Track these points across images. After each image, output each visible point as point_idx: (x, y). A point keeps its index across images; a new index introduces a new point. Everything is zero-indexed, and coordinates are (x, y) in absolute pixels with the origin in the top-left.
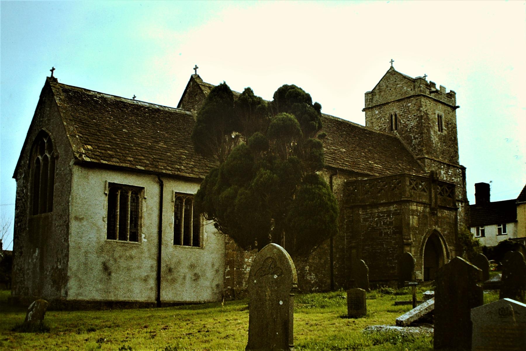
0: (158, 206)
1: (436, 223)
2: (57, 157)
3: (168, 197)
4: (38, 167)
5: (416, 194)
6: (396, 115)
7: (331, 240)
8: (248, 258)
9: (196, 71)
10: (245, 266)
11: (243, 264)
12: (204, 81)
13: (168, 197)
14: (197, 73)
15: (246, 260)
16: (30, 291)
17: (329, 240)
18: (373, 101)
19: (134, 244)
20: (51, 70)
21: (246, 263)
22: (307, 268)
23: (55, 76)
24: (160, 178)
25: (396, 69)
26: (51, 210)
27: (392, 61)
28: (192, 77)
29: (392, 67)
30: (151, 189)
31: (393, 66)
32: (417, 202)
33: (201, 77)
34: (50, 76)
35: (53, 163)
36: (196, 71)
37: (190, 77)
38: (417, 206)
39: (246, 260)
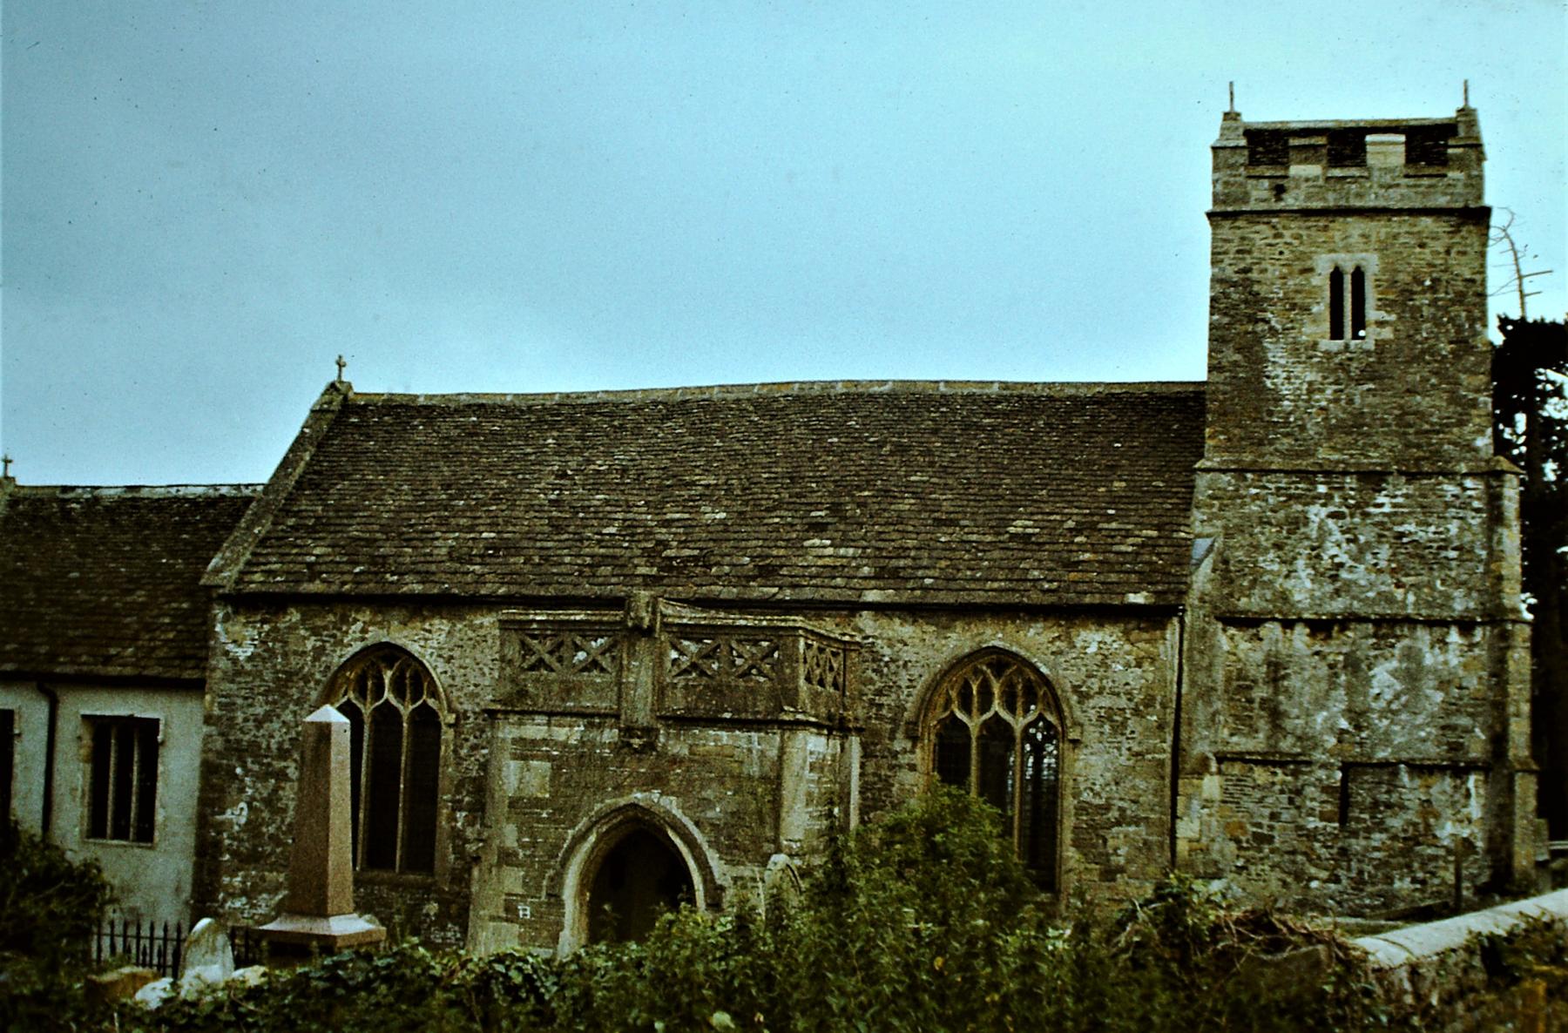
0: (44, 750)
1: (657, 780)
3: (70, 725)
5: (548, 683)
7: (1182, 622)
8: (233, 874)
10: (221, 896)
11: (216, 891)
13: (70, 725)
15: (226, 880)
16: (219, 818)
17: (1175, 620)
19: (1382, 143)
21: (225, 888)
22: (432, 908)
24: (50, 687)
30: (31, 713)
32: (550, 714)
38: (549, 724)
39: (226, 880)
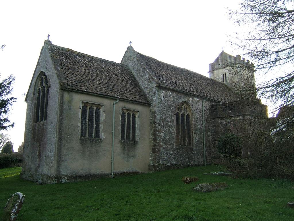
2: (50, 87)
4: (39, 94)
6: (226, 74)
9: (130, 44)
12: (53, 43)
14: (49, 40)
18: (213, 68)
20: (129, 43)
23: (50, 40)
25: (225, 52)
26: (46, 119)
27: (49, 36)
28: (128, 47)
29: (223, 51)
31: (224, 50)
33: (133, 47)
34: (47, 40)
35: (48, 90)
36: (130, 44)
37: (127, 47)
